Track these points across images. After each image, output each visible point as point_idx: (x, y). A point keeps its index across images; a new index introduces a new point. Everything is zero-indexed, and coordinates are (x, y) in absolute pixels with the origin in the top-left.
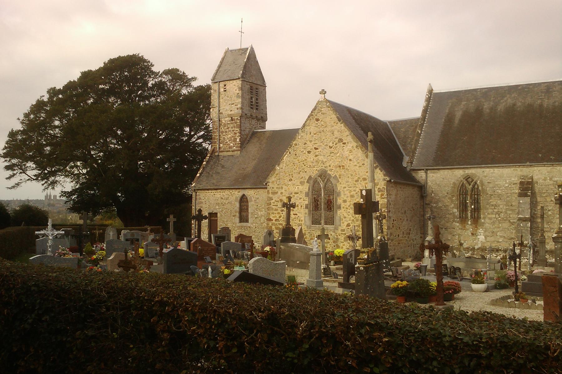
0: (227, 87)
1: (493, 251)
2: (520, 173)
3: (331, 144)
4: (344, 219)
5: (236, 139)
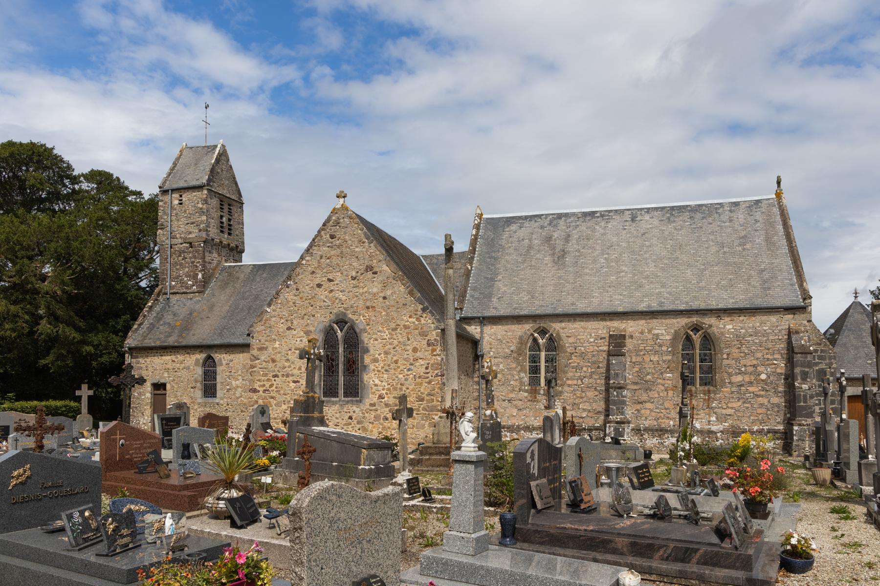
3: (354, 274)
5: (197, 275)
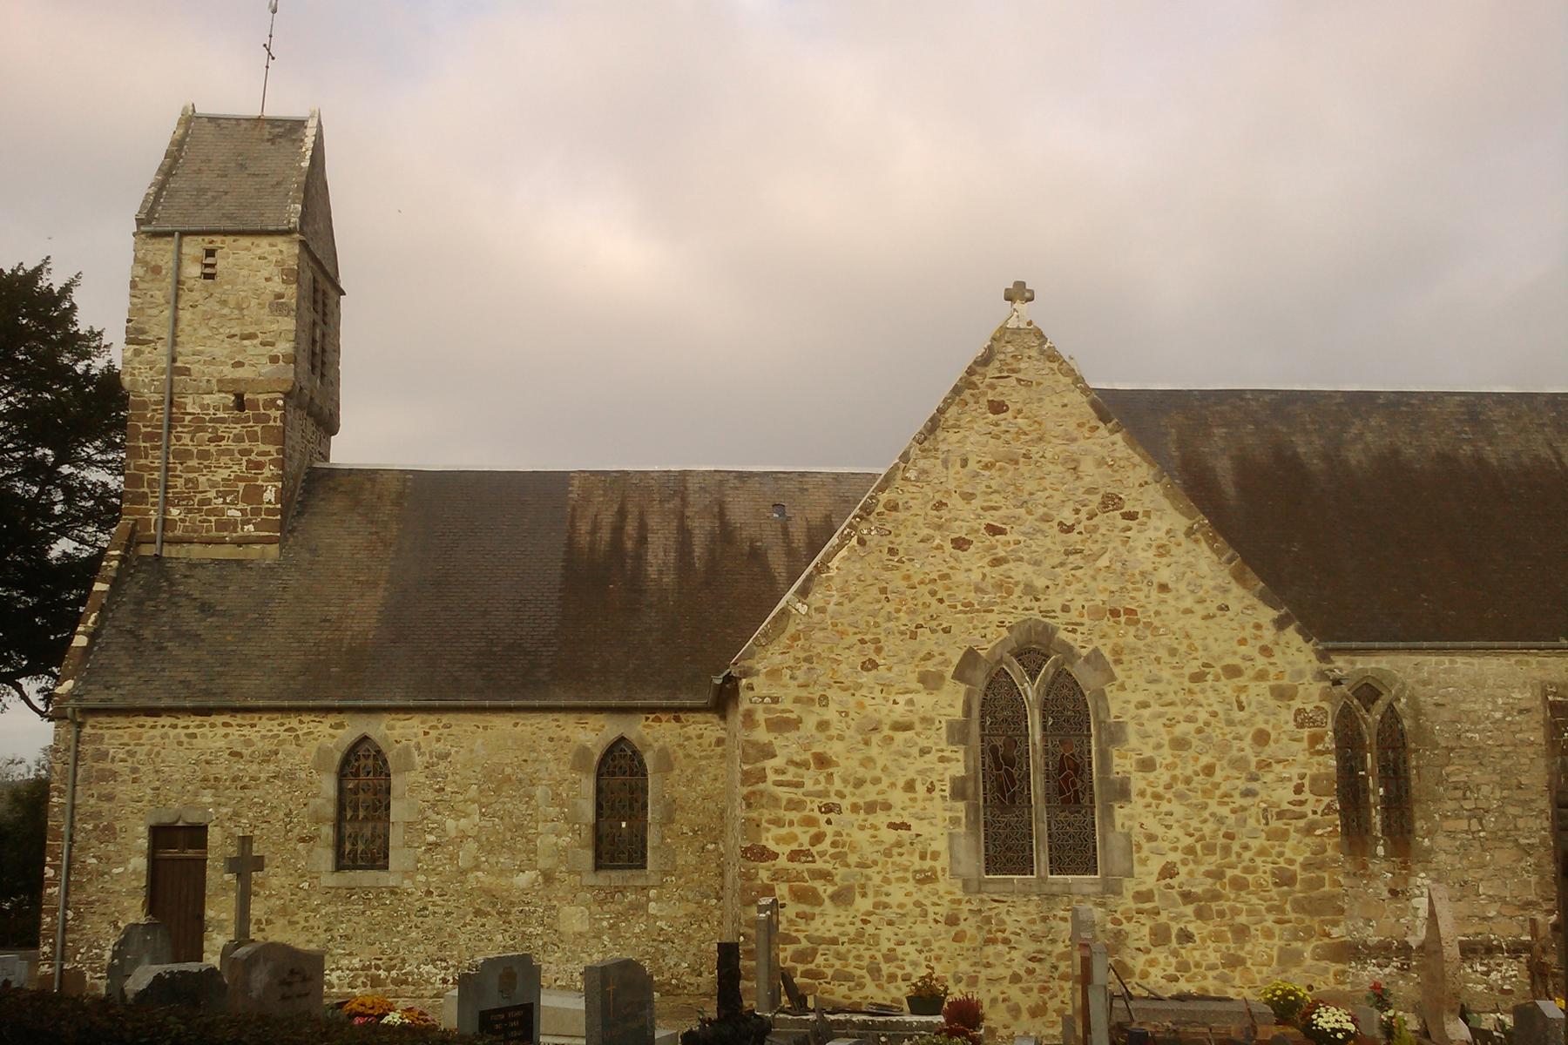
0: (222, 264)
1: (1474, 951)
2: (1537, 674)
3: (1068, 516)
4: (1146, 846)
5: (261, 490)
